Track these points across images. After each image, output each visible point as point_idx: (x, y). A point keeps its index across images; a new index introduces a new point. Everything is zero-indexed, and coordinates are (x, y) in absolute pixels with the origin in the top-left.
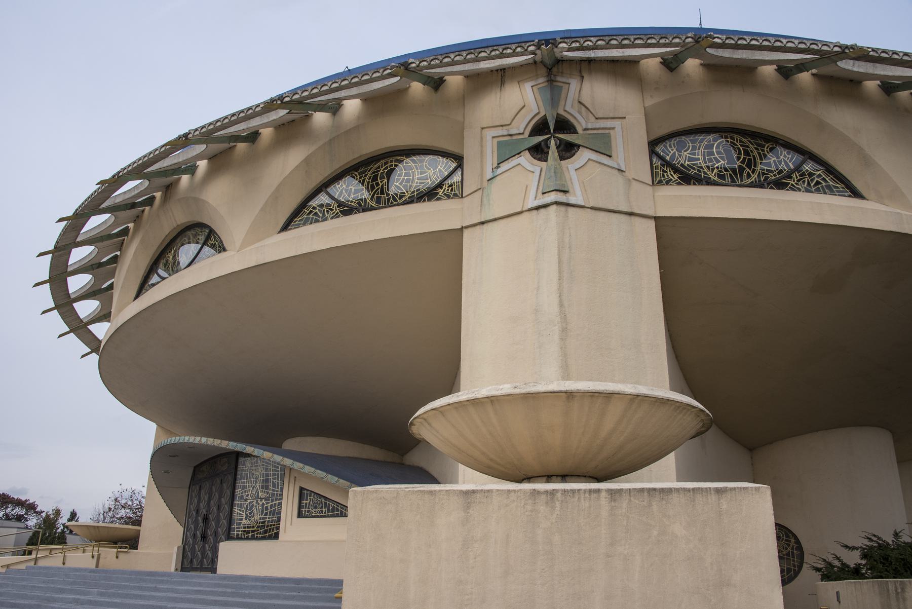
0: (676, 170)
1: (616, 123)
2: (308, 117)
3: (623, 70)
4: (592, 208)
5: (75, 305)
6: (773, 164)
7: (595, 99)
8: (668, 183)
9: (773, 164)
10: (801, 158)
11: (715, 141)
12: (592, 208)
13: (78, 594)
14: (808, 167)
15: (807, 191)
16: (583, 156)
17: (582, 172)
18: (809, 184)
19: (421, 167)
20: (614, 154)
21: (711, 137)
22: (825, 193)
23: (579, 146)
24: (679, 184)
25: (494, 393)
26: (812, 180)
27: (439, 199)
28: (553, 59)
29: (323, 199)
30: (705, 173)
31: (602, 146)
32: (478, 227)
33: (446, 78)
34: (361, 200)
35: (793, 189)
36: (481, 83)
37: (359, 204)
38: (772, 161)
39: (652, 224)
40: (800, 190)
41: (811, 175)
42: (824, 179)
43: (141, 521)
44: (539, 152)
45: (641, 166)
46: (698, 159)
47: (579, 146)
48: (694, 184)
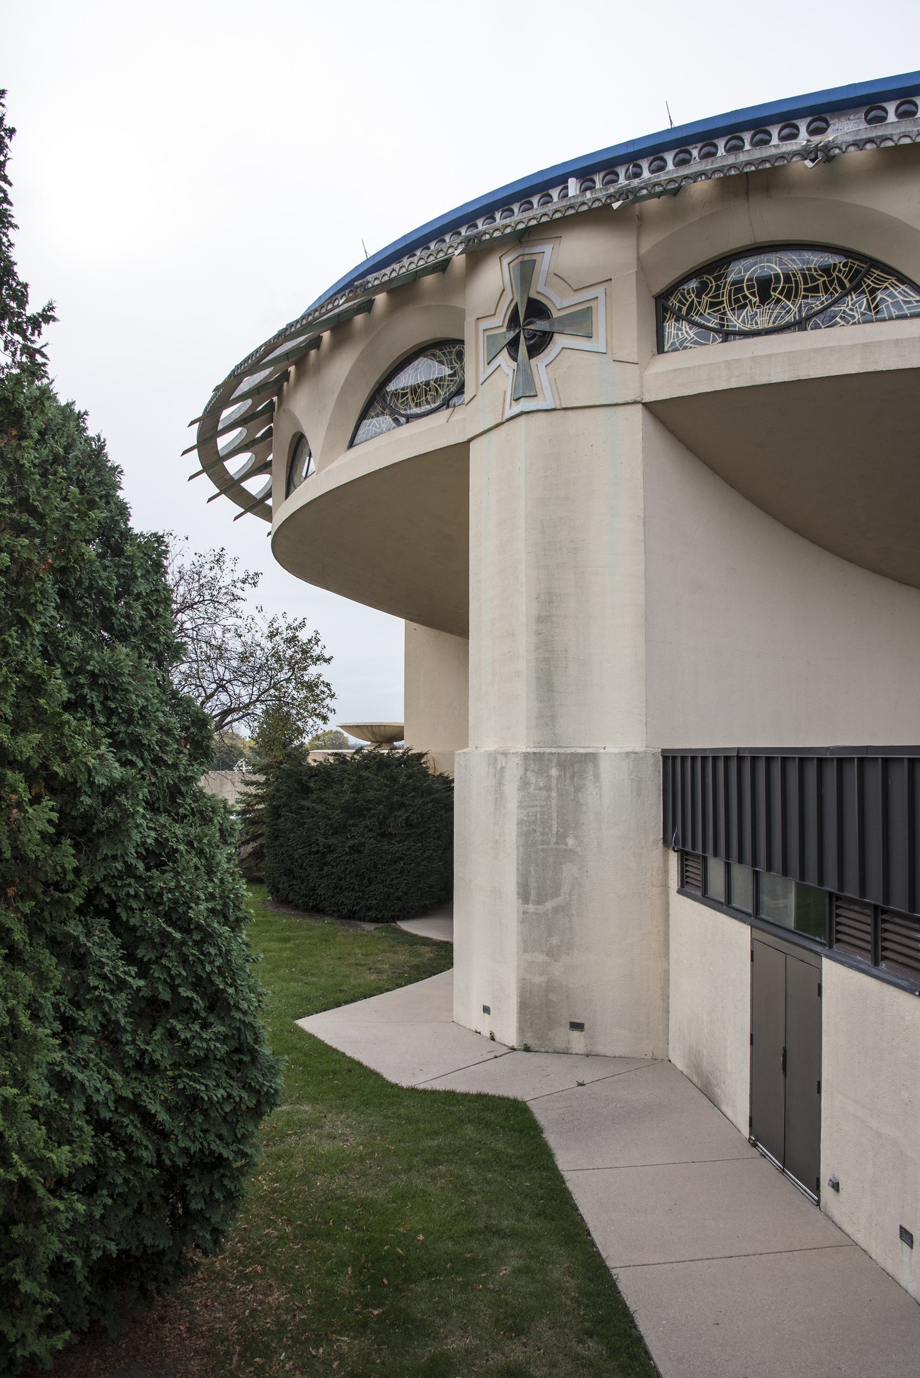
1: (599, 291)
16: (560, 341)
17: (567, 366)
31: (580, 322)
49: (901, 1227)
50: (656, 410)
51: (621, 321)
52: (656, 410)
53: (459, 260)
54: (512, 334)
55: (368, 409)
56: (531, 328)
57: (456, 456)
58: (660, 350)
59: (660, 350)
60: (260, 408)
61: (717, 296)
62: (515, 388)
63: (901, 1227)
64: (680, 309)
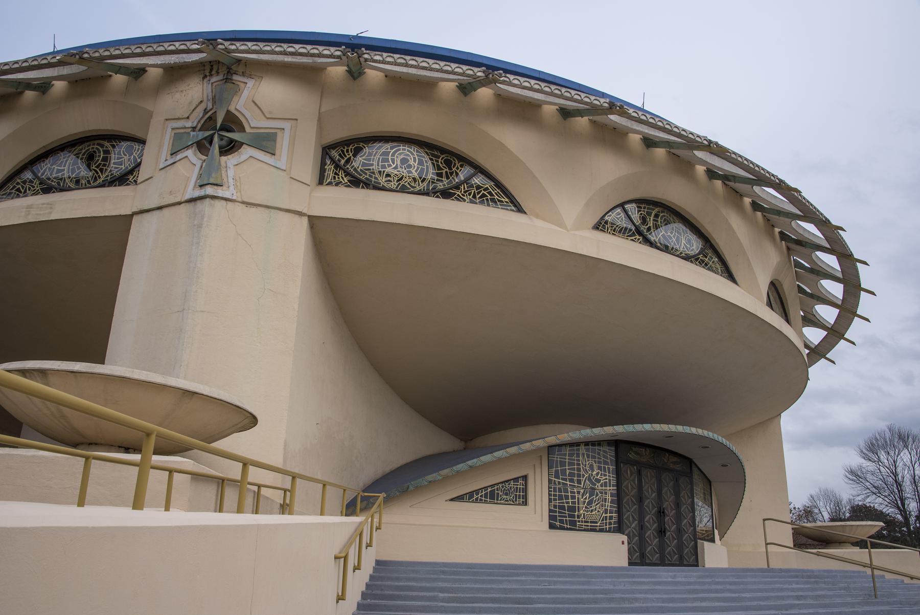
0: (347, 174)
1: (287, 125)
2: (21, 93)
3: (306, 75)
4: (243, 203)
5: (862, 292)
6: (444, 174)
7: (262, 99)
8: (337, 185)
9: (444, 174)
10: (472, 171)
11: (392, 148)
12: (243, 203)
13: (379, 599)
14: (478, 180)
15: (471, 202)
16: (246, 152)
17: (243, 170)
18: (474, 197)
19: (119, 153)
20: (277, 152)
21: (388, 146)
22: (488, 205)
23: (243, 144)
24: (348, 186)
25: (128, 375)
26: (479, 193)
27: (128, 184)
28: (221, 59)
29: (28, 175)
30: (376, 178)
31: (266, 142)
32: (155, 213)
33: (147, 69)
34: (61, 179)
35: (459, 199)
36: (175, 74)
37: (59, 184)
38: (444, 172)
39: (305, 220)
40: (465, 201)
41: (478, 187)
42: (490, 193)
43: (573, 526)
44: (202, 146)
45: (307, 167)
46: (372, 165)
47: (243, 144)
48: (363, 187)
49: (252, 421)
50: (314, 222)
51: (299, 155)
52: (314, 222)
53: (154, 74)
54: (201, 135)
55: (67, 147)
56: (220, 134)
57: (121, 225)
58: (321, 182)
59: (321, 182)
60: (806, 265)
61: (369, 160)
62: (200, 176)
63: (252, 421)
64: (339, 161)
